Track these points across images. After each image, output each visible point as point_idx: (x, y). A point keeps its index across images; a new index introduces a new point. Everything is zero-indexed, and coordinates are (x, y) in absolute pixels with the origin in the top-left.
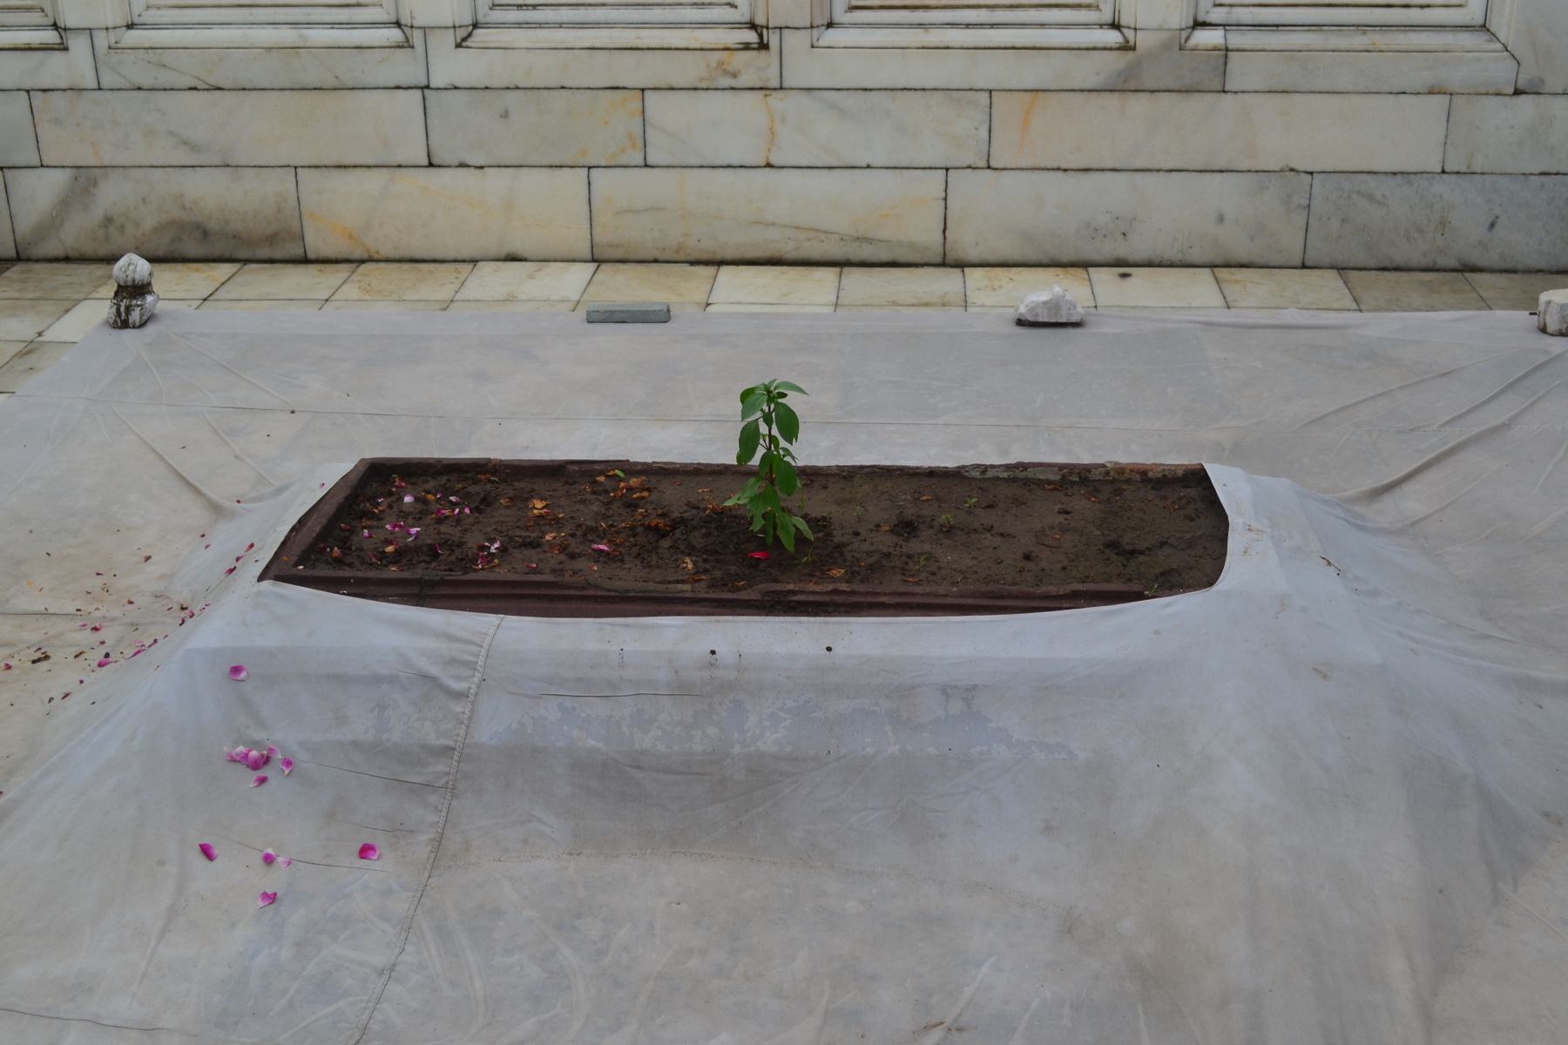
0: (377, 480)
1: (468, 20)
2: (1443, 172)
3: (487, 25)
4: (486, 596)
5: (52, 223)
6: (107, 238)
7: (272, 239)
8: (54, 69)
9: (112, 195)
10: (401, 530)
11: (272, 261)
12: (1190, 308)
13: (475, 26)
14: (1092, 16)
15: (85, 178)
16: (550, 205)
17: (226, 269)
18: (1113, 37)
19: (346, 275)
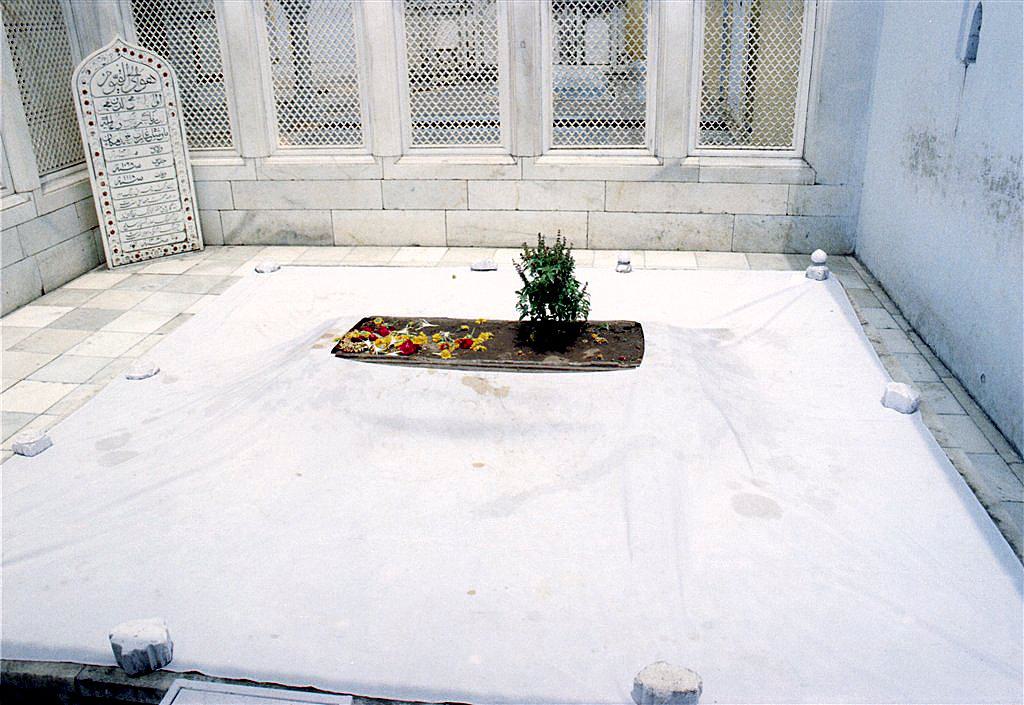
0: (365, 320)
1: (400, 153)
2: (15, 193)
3: (407, 155)
4: (394, 363)
5: (234, 234)
6: (259, 238)
7: (321, 237)
8: (242, 174)
9: (260, 220)
10: (370, 339)
11: (321, 246)
12: (332, 155)
13: (402, 156)
14: (646, 152)
15: (251, 215)
16: (431, 224)
17: (305, 248)
18: (655, 161)
19: (347, 252)
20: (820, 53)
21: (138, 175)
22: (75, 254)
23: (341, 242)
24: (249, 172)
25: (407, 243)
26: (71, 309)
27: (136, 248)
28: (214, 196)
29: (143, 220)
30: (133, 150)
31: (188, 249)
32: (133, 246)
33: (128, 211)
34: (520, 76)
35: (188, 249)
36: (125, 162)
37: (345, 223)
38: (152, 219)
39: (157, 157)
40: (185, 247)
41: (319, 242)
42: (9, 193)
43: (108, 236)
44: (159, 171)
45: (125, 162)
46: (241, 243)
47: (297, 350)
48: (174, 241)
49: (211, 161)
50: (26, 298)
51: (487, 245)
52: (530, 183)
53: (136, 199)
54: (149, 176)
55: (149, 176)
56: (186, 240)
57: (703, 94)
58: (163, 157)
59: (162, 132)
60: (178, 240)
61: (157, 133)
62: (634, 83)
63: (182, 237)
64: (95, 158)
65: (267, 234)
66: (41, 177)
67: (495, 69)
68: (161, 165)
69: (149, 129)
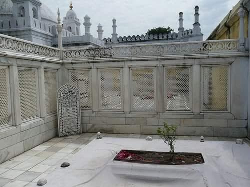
5: (89, 129)
15: (94, 125)
22: (51, 133)
34: (159, 93)
54: (71, 115)
55: (71, 115)
63: (77, 130)
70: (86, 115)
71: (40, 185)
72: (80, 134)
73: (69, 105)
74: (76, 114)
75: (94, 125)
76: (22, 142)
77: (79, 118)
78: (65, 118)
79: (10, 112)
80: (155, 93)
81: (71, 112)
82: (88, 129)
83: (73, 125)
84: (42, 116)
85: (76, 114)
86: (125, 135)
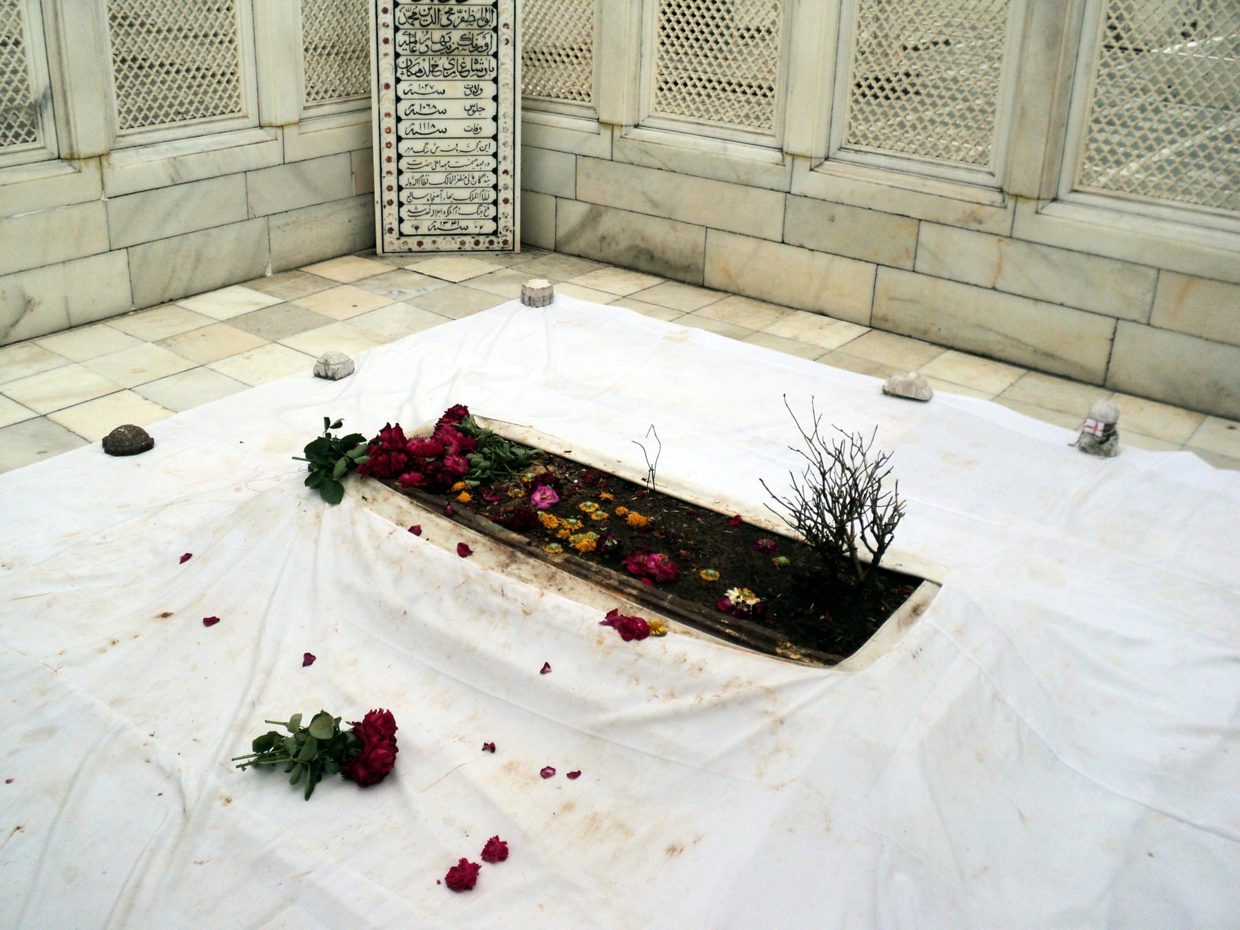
5: (571, 236)
7: (687, 269)
9: (608, 224)
11: (683, 282)
13: (827, 159)
15: (596, 212)
16: (850, 283)
17: (657, 280)
20: (1071, 17)
21: (440, 125)
22: (336, 225)
23: (715, 284)
24: (601, 145)
25: (810, 307)
26: (280, 301)
27: (420, 232)
28: (554, 170)
29: (437, 192)
30: (439, 86)
31: (496, 246)
32: (417, 228)
33: (418, 176)
34: (1036, 45)
35: (496, 246)
36: (424, 103)
37: (728, 257)
38: (450, 192)
39: (473, 102)
40: (491, 242)
41: (680, 276)
42: (252, 124)
43: (383, 207)
44: (471, 123)
45: (424, 103)
46: (576, 252)
47: (1117, 418)
48: (477, 231)
49: (565, 121)
50: (239, 274)
51: (934, 339)
52: (1023, 247)
53: (431, 160)
54: (456, 129)
55: (456, 129)
56: (495, 233)
57: (23, 52)
58: (481, 103)
59: (486, 65)
60: (483, 231)
61: (479, 67)
62: (1207, 85)
63: (489, 227)
64: (383, 92)
65: (613, 246)
66: (305, 108)
67: (1109, 47)
68: (477, 115)
69: (468, 60)
70: (567, 128)
71: (326, 377)
72: (506, 251)
73: (443, 62)
74: (489, 128)
75: (596, 212)
76: (120, 258)
77: (505, 151)
78: (418, 145)
79: (37, 82)
80: (1007, 69)
81: (456, 109)
82: (563, 231)
83: (464, 194)
84: (265, 121)
85: (489, 128)
86: (759, 318)
